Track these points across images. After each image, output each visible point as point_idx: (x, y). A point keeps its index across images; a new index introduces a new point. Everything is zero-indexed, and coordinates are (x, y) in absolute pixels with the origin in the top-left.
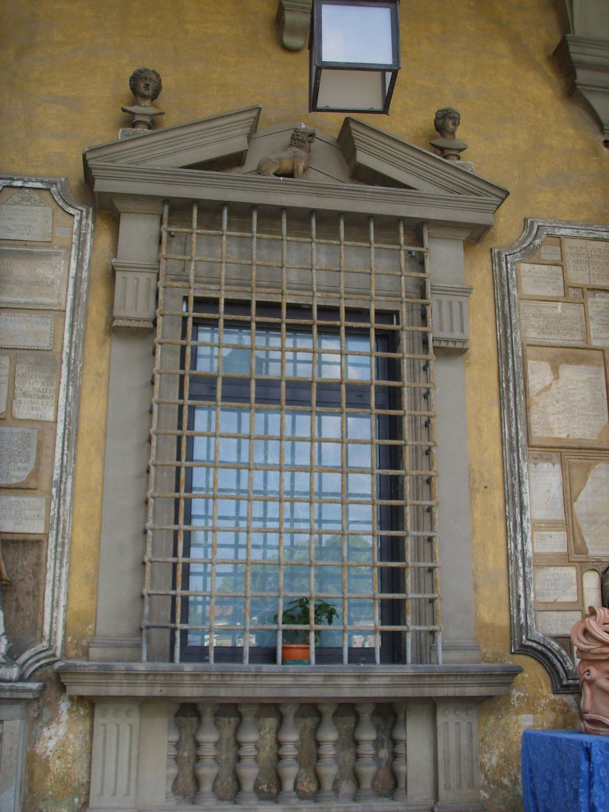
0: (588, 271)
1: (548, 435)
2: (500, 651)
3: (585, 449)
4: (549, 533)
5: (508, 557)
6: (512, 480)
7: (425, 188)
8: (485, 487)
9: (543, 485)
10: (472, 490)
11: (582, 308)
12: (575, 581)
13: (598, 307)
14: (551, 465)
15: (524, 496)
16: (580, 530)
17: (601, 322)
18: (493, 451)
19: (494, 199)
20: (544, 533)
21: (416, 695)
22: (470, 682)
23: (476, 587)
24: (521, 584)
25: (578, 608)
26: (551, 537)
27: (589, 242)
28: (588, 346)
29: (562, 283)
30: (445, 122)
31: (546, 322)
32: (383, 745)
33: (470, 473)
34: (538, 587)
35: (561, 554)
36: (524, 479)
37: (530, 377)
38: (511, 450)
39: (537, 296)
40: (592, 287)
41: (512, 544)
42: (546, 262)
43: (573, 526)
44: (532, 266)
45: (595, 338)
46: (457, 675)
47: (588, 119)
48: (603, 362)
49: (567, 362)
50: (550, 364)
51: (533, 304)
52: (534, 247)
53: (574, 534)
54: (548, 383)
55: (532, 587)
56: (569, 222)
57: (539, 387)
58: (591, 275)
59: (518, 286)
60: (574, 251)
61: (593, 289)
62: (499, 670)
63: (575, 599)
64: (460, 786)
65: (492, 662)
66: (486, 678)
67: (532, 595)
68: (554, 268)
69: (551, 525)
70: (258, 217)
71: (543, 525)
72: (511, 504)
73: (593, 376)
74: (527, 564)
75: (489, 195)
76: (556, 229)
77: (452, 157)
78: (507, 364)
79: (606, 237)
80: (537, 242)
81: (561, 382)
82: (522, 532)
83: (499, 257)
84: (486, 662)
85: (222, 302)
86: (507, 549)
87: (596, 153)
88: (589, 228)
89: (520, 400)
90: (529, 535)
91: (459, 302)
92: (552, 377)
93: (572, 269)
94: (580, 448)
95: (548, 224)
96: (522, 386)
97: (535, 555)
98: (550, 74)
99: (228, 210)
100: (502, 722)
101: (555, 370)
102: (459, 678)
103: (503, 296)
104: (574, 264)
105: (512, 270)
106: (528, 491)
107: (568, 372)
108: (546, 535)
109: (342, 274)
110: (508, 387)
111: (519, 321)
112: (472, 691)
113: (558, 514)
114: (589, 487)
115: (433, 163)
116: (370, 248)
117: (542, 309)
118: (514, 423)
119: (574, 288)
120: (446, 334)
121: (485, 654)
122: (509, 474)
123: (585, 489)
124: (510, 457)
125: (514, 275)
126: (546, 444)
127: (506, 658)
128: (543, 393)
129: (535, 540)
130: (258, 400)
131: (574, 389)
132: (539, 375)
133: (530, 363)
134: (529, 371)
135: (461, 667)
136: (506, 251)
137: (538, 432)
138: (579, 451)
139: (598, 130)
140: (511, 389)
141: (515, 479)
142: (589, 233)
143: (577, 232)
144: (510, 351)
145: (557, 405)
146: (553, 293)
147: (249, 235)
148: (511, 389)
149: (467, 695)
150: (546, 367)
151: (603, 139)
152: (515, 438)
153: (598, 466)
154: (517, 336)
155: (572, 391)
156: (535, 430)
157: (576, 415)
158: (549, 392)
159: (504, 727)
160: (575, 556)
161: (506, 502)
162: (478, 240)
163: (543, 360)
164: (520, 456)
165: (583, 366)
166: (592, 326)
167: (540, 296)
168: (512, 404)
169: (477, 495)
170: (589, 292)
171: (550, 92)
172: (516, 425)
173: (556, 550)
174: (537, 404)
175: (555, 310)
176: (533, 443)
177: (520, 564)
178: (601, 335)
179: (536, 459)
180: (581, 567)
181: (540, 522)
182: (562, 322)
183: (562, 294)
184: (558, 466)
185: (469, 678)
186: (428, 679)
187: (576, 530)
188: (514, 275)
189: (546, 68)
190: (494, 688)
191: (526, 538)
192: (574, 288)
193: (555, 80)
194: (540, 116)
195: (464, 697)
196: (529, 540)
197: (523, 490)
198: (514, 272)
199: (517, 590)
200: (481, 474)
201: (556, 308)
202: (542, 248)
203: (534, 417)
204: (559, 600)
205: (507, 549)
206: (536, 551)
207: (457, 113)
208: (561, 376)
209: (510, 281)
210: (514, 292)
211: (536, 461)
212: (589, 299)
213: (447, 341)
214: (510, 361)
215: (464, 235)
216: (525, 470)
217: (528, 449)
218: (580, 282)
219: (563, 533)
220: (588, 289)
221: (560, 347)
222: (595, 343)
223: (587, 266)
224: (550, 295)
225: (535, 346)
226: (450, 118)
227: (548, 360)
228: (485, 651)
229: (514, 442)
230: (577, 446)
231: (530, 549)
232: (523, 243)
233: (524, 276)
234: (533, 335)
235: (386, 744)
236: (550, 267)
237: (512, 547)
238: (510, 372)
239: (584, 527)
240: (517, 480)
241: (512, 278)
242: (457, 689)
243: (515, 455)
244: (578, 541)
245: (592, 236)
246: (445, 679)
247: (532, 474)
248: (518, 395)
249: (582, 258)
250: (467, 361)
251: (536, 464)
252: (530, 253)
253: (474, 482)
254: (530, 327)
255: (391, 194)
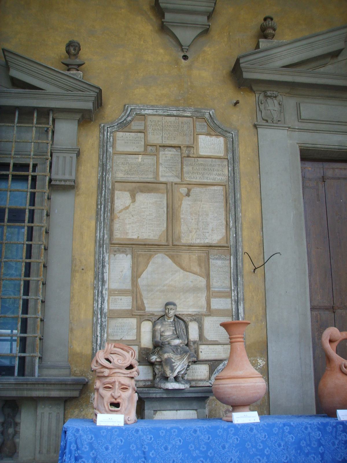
0: (161, 135)
1: (125, 237)
2: (85, 370)
3: (148, 245)
4: (120, 297)
5: (94, 312)
6: (98, 266)
7: (50, 88)
8: (83, 269)
9: (119, 268)
10: (73, 271)
11: (155, 158)
12: (135, 327)
13: (166, 157)
14: (125, 255)
15: (105, 274)
16: (141, 295)
17: (167, 166)
18: (90, 247)
19: (92, 93)
20: (116, 297)
21: (45, 395)
22: (53, 388)
23: (71, 330)
24: (99, 328)
25: (135, 344)
26: (121, 299)
27: (164, 117)
28: (158, 182)
29: (143, 143)
30: (73, 48)
31: (130, 167)
32: (11, 425)
33: (72, 261)
34: (110, 331)
35: (127, 310)
36: (106, 264)
37: (116, 201)
38: (100, 247)
39: (126, 152)
40: (163, 145)
41: (96, 304)
42: (134, 131)
43: (137, 293)
44: (124, 133)
45: (162, 176)
46: (44, 384)
47: (174, 43)
48: (166, 191)
49: (142, 191)
50: (130, 193)
51: (122, 156)
52: (126, 122)
53: (137, 298)
54: (127, 205)
55: (106, 330)
56: (152, 106)
57: (121, 207)
58: (164, 138)
59: (113, 146)
60: (153, 123)
61: (164, 146)
62: (70, 381)
63: (135, 338)
64: (48, 452)
65: (80, 376)
66: (63, 386)
67: (106, 335)
68: (139, 134)
69: (122, 292)
70: (19, 114)
71: (116, 292)
72: (97, 280)
73: (158, 200)
74: (103, 316)
75: (89, 91)
76: (142, 110)
77: (72, 69)
78: (102, 194)
79: (175, 114)
80: (129, 118)
81: (136, 204)
82: (102, 297)
83: (104, 129)
84: (75, 376)
85: (11, 166)
86: (93, 307)
87: (177, 63)
88: (165, 109)
89: (107, 216)
90: (106, 299)
91: (70, 157)
92: (131, 201)
93: (150, 134)
94: (145, 245)
95: (137, 108)
96: (109, 207)
97: (110, 311)
98: (152, 17)
99: (19, 112)
100: (83, 413)
101: (133, 197)
102: (45, 386)
103: (103, 152)
104: (153, 131)
105: (110, 137)
106: (108, 271)
107: (141, 197)
108: (118, 299)
109: (33, 144)
110: (101, 208)
111: (112, 167)
112: (200, 395)
113: (128, 286)
114: (150, 268)
115: (55, 74)
116: (14, 126)
117: (128, 159)
118: (102, 230)
119: (151, 146)
120: (60, 177)
121: (75, 371)
122: (97, 261)
123: (146, 270)
124: (99, 250)
125: (111, 140)
126: (122, 242)
127: (88, 374)
128: (124, 211)
129: (110, 301)
130: (9, 221)
131: (145, 208)
132: (122, 199)
133: (116, 192)
134: (116, 197)
135: (46, 379)
136: (108, 125)
137: (118, 235)
138: (144, 246)
139: (180, 49)
140: (102, 209)
141: (100, 264)
142: (164, 112)
143: (156, 112)
144: (103, 186)
145: (133, 218)
146: (137, 150)
147: (31, 125)
148: (102, 209)
149: (52, 396)
150: (127, 194)
151: (182, 54)
152: (102, 239)
153: (157, 255)
154: (109, 177)
155: (144, 210)
156: (117, 234)
157: (145, 224)
158: (127, 211)
159: (84, 416)
160: (136, 311)
161: (95, 278)
162: (90, 120)
163: (125, 191)
164: (104, 250)
165: (152, 194)
166: (161, 169)
167: (128, 152)
168: (102, 218)
169: (77, 274)
170: (161, 148)
171: (150, 28)
172: (104, 231)
173: (124, 308)
174: (119, 218)
175: (137, 160)
176: (114, 242)
177: (99, 316)
178: (167, 175)
179: (115, 251)
180: (140, 318)
181: (115, 290)
182: (141, 167)
183: (143, 149)
184: (129, 256)
185: (53, 386)
186: (25, 386)
187: (138, 296)
188: (111, 140)
189: (150, 14)
190: (69, 392)
191: (104, 300)
192: (151, 146)
193: (155, 20)
194: (142, 43)
195: (49, 397)
196: (106, 302)
197: (105, 271)
198: (111, 138)
199: (97, 332)
200: (80, 261)
201: (138, 158)
202: (133, 123)
203: (117, 225)
204: (123, 339)
205: (93, 307)
206: (110, 308)
207: (77, 43)
208: (136, 200)
209: (109, 143)
210: (110, 150)
211: (116, 253)
212: (160, 152)
213: (60, 180)
214: (103, 192)
215: (78, 116)
216: (107, 259)
217: (110, 245)
218: (156, 142)
219: (129, 297)
220: (160, 146)
221: (138, 182)
222: (162, 179)
223: (161, 133)
224: (134, 150)
225: (121, 182)
226: (72, 46)
227: (129, 191)
228: (75, 369)
229: (101, 242)
230: (143, 243)
231: (106, 307)
232: (120, 119)
233: (119, 140)
234: (120, 176)
235: (13, 425)
236: (136, 133)
237: (96, 306)
238: (103, 199)
239: (144, 294)
240: (101, 265)
241: (110, 141)
242: (45, 392)
243: (101, 249)
244: (139, 302)
245: (166, 113)
246: (37, 386)
247: (112, 261)
248: (106, 213)
249: (158, 128)
250: (77, 193)
251: (115, 255)
252: (124, 126)
253: (76, 266)
254: (120, 171)
255: (26, 94)
